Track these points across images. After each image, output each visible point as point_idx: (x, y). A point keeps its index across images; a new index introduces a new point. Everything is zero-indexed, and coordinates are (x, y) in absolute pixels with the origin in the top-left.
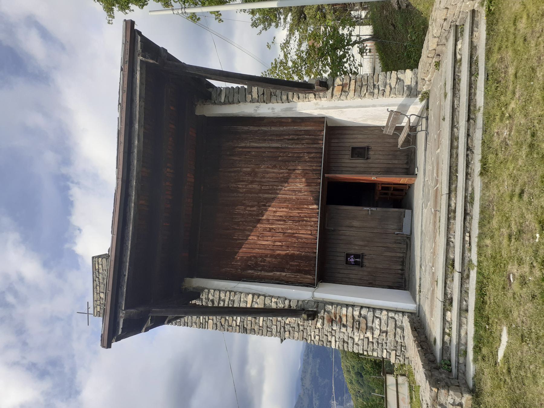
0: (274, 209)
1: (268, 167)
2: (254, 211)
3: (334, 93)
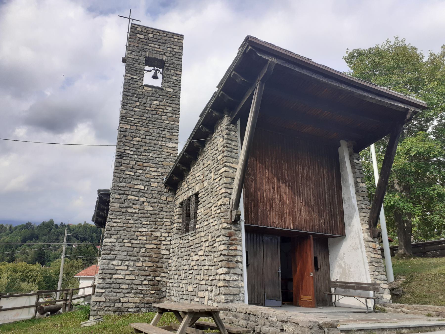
0: (287, 193)
1: (313, 190)
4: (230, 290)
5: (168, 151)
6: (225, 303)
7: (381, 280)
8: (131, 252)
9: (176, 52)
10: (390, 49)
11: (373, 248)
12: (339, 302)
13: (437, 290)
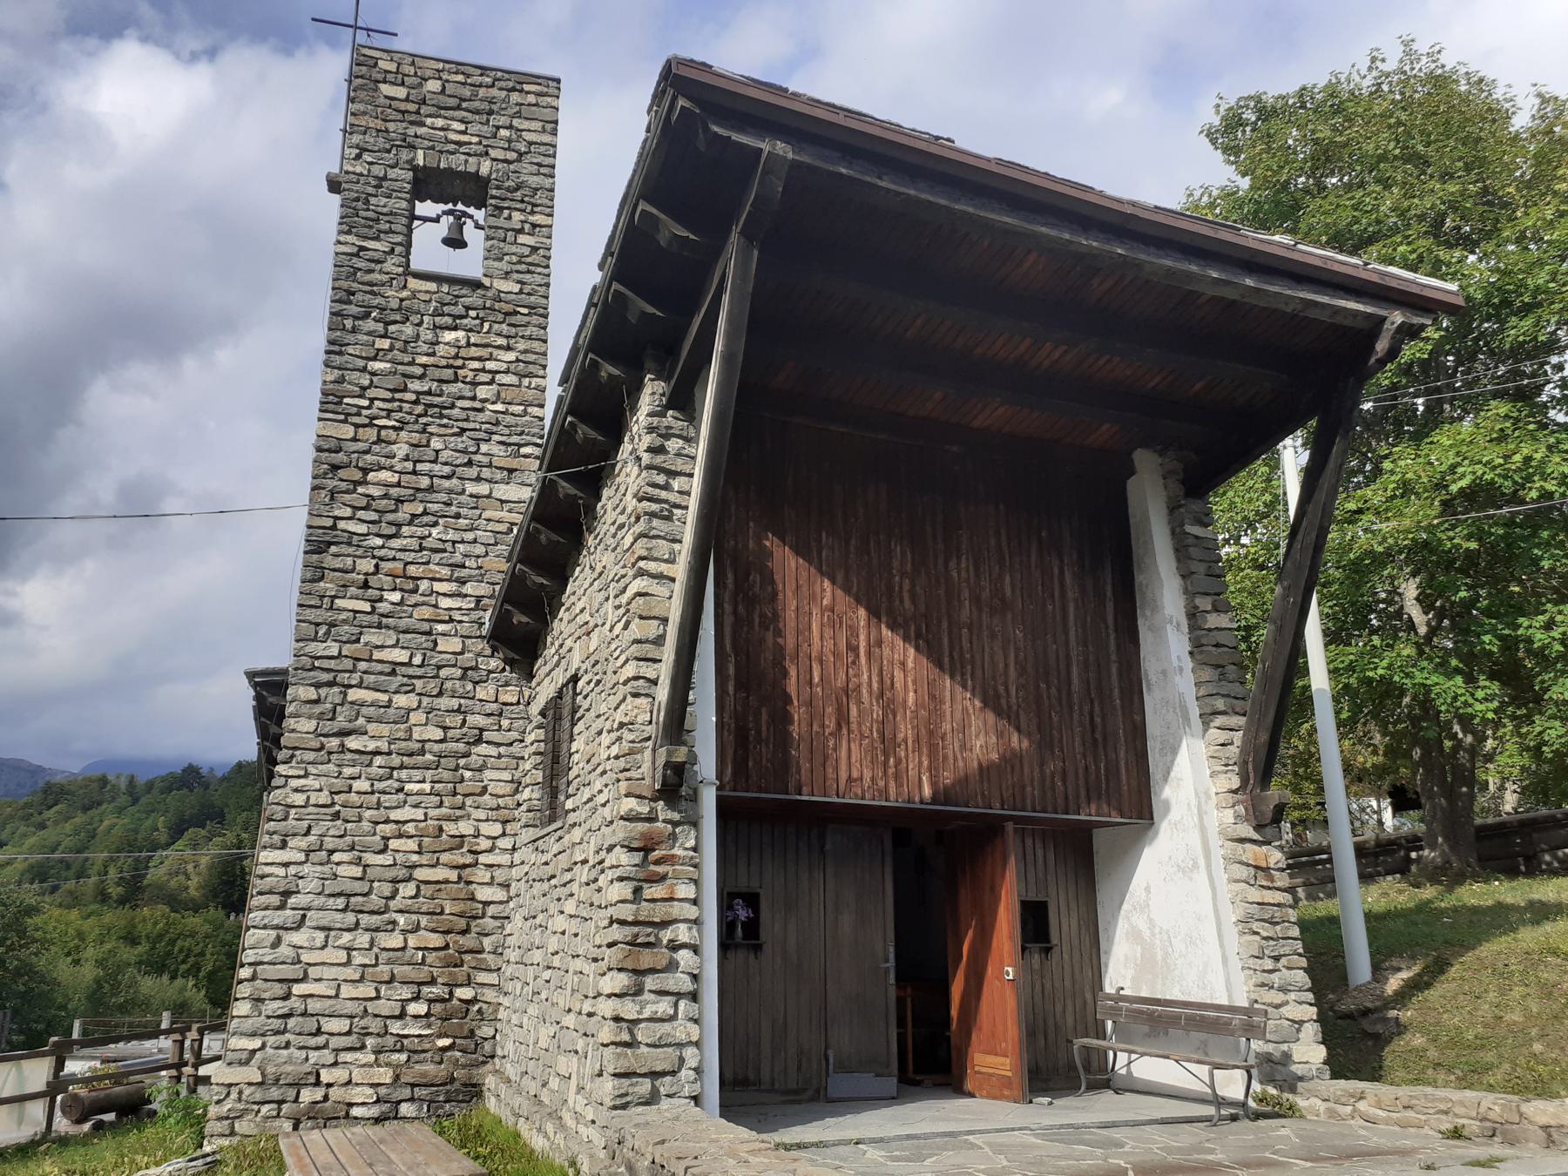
0: (910, 665)
1: (1017, 650)
2: (902, 601)
3: (1248, 846)
4: (636, 1057)
5: (504, 514)
6: (615, 1108)
7: (1284, 990)
8: (360, 899)
9: (531, 143)
10: (1385, 88)
11: (1256, 867)
12: (1129, 1073)
13: (1528, 1016)
